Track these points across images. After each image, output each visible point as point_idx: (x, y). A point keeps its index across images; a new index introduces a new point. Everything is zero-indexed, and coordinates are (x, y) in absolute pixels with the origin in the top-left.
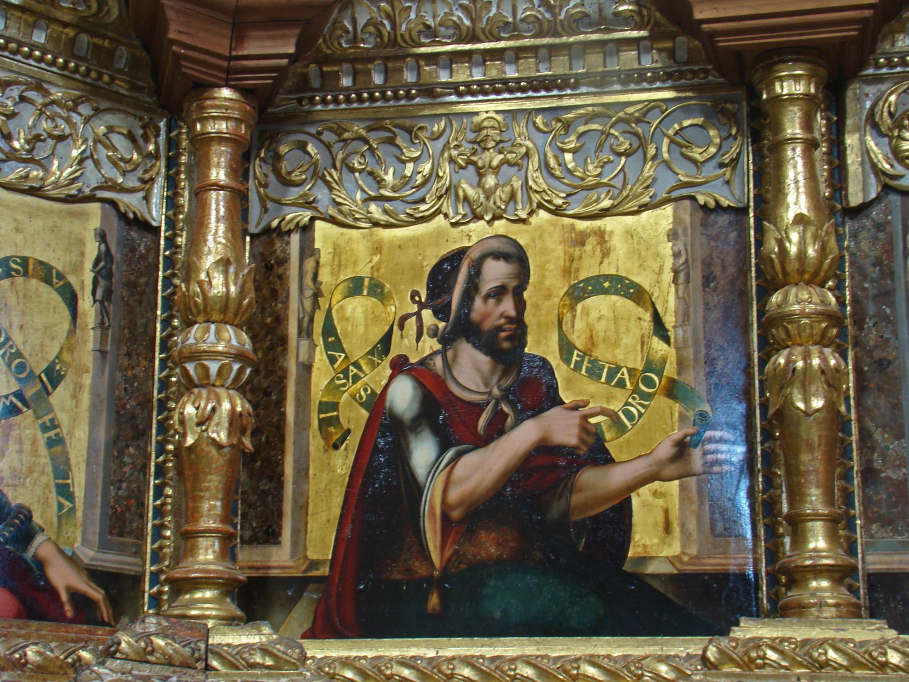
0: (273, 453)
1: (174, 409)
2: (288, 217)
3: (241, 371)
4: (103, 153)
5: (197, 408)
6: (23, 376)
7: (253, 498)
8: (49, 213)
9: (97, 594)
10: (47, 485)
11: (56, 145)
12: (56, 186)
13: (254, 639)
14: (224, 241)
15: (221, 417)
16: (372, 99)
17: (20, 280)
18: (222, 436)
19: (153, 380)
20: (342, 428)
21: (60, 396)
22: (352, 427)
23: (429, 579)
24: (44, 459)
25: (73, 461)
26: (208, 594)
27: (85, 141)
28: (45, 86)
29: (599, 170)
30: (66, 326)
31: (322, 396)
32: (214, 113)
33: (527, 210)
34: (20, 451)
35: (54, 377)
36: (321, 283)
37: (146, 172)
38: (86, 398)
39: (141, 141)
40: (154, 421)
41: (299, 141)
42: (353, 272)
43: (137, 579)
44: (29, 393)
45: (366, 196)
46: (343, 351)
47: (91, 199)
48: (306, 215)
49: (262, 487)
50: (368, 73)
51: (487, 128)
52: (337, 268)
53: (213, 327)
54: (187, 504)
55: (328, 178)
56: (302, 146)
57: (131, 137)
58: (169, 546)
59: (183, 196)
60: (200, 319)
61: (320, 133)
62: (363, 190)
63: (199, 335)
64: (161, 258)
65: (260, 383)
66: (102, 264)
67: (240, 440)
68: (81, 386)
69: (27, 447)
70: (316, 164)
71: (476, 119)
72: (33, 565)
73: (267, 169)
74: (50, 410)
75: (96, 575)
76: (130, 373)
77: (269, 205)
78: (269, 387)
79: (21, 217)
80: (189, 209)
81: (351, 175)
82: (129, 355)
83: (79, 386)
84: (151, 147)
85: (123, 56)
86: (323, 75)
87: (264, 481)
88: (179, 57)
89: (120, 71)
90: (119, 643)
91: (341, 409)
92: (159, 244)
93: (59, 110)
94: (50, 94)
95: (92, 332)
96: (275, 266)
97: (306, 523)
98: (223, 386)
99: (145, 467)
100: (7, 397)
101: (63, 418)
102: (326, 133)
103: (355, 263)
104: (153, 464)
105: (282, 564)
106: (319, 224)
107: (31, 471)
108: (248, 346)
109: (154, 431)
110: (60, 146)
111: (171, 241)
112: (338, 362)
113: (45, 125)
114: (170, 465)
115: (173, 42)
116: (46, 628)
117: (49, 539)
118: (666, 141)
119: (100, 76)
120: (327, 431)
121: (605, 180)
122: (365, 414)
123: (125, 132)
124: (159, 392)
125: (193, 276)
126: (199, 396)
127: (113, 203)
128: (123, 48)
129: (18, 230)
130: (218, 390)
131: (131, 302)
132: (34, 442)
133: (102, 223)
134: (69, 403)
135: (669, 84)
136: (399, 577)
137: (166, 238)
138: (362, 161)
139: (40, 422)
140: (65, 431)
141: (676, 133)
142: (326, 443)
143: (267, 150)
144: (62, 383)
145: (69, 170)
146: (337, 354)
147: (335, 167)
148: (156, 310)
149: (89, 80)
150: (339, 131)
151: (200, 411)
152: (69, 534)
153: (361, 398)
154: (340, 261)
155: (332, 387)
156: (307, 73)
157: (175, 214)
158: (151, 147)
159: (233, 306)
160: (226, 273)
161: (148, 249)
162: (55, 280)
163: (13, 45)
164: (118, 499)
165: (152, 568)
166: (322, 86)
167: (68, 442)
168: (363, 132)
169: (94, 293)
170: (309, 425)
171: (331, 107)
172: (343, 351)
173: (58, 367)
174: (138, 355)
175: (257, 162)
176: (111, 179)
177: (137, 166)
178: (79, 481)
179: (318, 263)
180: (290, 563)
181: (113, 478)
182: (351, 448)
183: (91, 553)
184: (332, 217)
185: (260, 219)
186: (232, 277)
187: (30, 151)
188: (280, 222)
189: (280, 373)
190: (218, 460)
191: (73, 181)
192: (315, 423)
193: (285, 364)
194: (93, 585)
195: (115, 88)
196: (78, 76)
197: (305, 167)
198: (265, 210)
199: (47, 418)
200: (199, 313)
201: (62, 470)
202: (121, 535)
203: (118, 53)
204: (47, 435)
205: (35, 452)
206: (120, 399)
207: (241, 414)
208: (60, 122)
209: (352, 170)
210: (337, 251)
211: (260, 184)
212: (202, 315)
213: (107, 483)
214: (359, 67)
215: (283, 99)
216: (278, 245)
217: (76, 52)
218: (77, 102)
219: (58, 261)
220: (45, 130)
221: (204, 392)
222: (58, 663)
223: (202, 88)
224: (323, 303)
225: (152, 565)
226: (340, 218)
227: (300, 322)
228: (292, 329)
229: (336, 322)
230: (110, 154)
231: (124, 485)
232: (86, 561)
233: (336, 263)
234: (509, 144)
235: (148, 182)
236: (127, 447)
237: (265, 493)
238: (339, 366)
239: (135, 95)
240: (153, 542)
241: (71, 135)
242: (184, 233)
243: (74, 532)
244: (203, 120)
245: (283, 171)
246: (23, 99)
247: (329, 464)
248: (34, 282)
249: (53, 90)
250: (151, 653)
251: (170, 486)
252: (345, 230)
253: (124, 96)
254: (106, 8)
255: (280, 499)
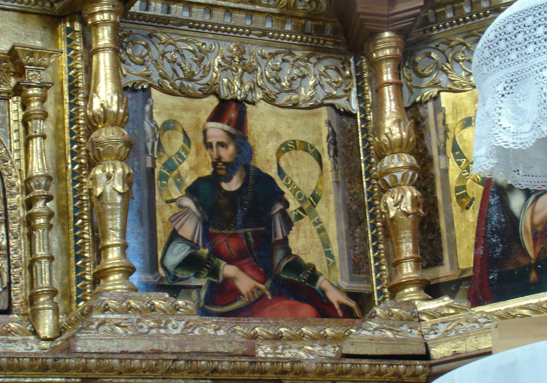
0: (433, 219)
1: (379, 205)
2: (425, 94)
3: (413, 175)
4: (324, 80)
5: (393, 198)
6: (301, 199)
7: (425, 244)
8: (302, 116)
9: (352, 304)
10: (321, 252)
11: (301, 81)
12: (304, 101)
13: (443, 304)
14: (395, 111)
15: (406, 200)
16: (465, 21)
17: (293, 152)
18: (409, 209)
19: (364, 193)
20: (469, 198)
21: (320, 207)
22: (475, 196)
23: (530, 266)
24: (317, 239)
25: (331, 239)
26: (412, 289)
27: (315, 76)
28: (293, 52)
30: (318, 171)
31: (456, 184)
32: (381, 46)
34: (305, 237)
35: (316, 198)
36: (447, 125)
37: (346, 86)
38: (332, 206)
39: (342, 71)
40: (367, 214)
41: (426, 53)
42: (465, 115)
43: (371, 295)
44: (305, 207)
45: (467, 73)
46: (465, 158)
47: (322, 105)
48: (434, 91)
49: (429, 238)
50: (461, 7)
52: (455, 115)
53: (396, 156)
54: (393, 247)
55: (445, 68)
56: (429, 55)
57: (337, 70)
58: (385, 274)
59: (368, 94)
60: (389, 152)
62: (465, 71)
63: (389, 161)
64: (359, 129)
65: (420, 184)
66: (331, 138)
67: (418, 210)
68: (329, 200)
69: (309, 234)
70: (437, 63)
72: (320, 292)
73: (411, 71)
74: (317, 214)
75: (351, 295)
76: (352, 191)
77: (414, 90)
78: (426, 185)
79: (290, 120)
80: (372, 100)
81: (457, 64)
82: (350, 182)
83: (328, 201)
84: (348, 73)
85: (329, 28)
86: (436, 14)
87: (430, 235)
88: (363, 20)
89: (328, 37)
90: (376, 312)
91: (467, 188)
92: (357, 123)
93: (300, 63)
94: (294, 55)
95: (330, 173)
96: (421, 121)
97: (456, 251)
98: (404, 185)
99: (366, 238)
100: (295, 211)
101: (323, 218)
102: (441, 45)
103: (466, 110)
104: (370, 236)
105: (446, 275)
106: (442, 94)
107: (312, 246)
108: (415, 162)
109: (368, 219)
110: (304, 81)
111: (364, 120)
112: (463, 164)
113: (296, 71)
114: (380, 233)
115: (359, 14)
116: (332, 320)
117: (325, 279)
119: (319, 40)
120: (462, 202)
122: (481, 188)
123: (334, 68)
124: (368, 198)
125: (382, 131)
126: (393, 192)
127: (332, 105)
128: (328, 24)
129: (289, 127)
130: (403, 187)
131: (347, 155)
132: (311, 231)
133: (328, 117)
134: (325, 210)
135: (93, 32)
136: (513, 267)
137: (361, 119)
138: (463, 55)
139: (312, 221)
140: (325, 224)
142: (462, 207)
143: (409, 61)
144: (320, 201)
145: (310, 92)
146: (461, 160)
147: (448, 62)
148: (360, 156)
149: (313, 45)
150: (448, 42)
151: (395, 199)
152: (334, 275)
153: (478, 179)
154: (457, 111)
155: (462, 178)
156: (427, 16)
157: (365, 105)
158: (348, 73)
159: (405, 144)
160: (399, 126)
161: (352, 126)
162: (310, 149)
163: (276, 34)
164: (355, 255)
165: (378, 288)
166: (436, 20)
167: (327, 229)
168: (462, 40)
169: (329, 153)
170: (451, 200)
171: (442, 30)
172: (465, 158)
173: (317, 193)
174: (354, 181)
175: (405, 69)
176: (330, 93)
177: (342, 84)
178: (335, 248)
179: (444, 115)
180: (451, 273)
181: (351, 247)
182: (476, 207)
183: (346, 284)
184: (449, 88)
185: (410, 98)
186: (402, 128)
187: (290, 86)
188: (421, 98)
189: (431, 177)
190: (408, 222)
191: (312, 97)
192: (454, 199)
193: (433, 172)
194: (349, 299)
195: (326, 46)
196: (308, 44)
197: (432, 65)
198: (412, 93)
199: (315, 219)
200: (387, 149)
201: (326, 244)
202: (359, 274)
203: (326, 27)
204: (317, 227)
205: (312, 236)
206: (349, 205)
207: (417, 197)
208: (302, 69)
209: (458, 61)
210: (455, 107)
211: (407, 80)
212: (389, 150)
213: (349, 248)
214: (456, 5)
215: (415, 33)
216: (421, 111)
217: (306, 31)
218: (309, 56)
219: (309, 139)
220: (296, 74)
221: (396, 190)
222: (342, 335)
223: (374, 35)
224: (450, 135)
225: (377, 286)
226: (455, 88)
227: (439, 148)
228: (435, 152)
229: (459, 143)
230: (328, 80)
231: (357, 248)
232: (344, 288)
233: (455, 112)
235: (348, 91)
236: (356, 229)
237: (431, 241)
238: (464, 166)
239: (336, 47)
240: (376, 274)
241: (308, 74)
242: (371, 113)
243: (336, 274)
244: (376, 51)
245: (420, 71)
246: (284, 61)
247: (465, 218)
248: (300, 152)
249: (297, 53)
250: (392, 316)
251: (382, 244)
252: (460, 94)
253: (331, 49)
254: (320, 5)
255: (440, 242)
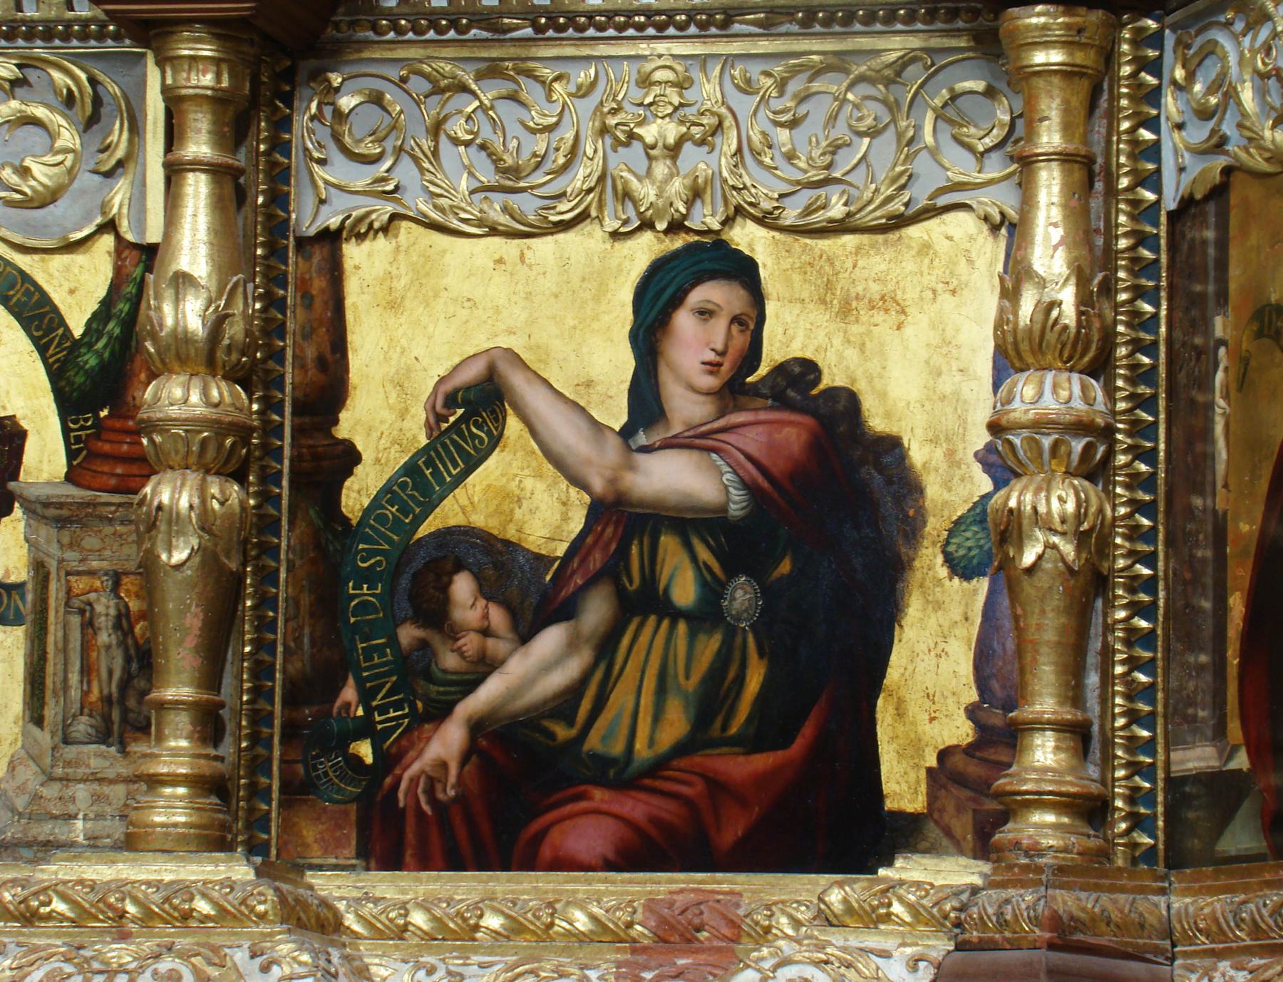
29: (828, 158)
33: (720, 217)
45: (476, 185)
51: (660, 83)
61: (404, 80)
71: (648, 67)
81: (454, 148)
118: (930, 117)
121: (837, 174)
141: (945, 105)
234: (694, 110)
